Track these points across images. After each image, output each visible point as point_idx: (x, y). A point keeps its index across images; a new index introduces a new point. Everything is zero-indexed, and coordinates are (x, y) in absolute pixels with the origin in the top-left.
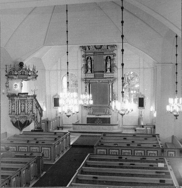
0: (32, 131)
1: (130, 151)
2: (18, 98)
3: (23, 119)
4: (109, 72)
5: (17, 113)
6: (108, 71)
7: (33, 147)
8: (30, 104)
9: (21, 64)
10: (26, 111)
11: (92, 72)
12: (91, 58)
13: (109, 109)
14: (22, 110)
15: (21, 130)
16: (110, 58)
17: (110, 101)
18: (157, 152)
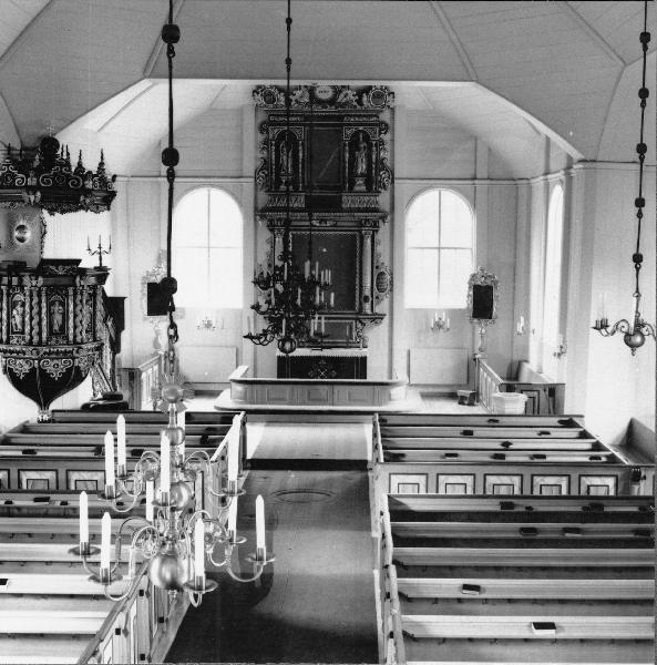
0: (86, 408)
1: (516, 480)
2: (40, 279)
3: (56, 361)
4: (364, 188)
5: (36, 339)
6: (360, 185)
7: (590, 478)
8: (87, 301)
10: (71, 331)
13: (359, 325)
14: (56, 328)
15: (43, 403)
16: (367, 138)
17: (366, 299)
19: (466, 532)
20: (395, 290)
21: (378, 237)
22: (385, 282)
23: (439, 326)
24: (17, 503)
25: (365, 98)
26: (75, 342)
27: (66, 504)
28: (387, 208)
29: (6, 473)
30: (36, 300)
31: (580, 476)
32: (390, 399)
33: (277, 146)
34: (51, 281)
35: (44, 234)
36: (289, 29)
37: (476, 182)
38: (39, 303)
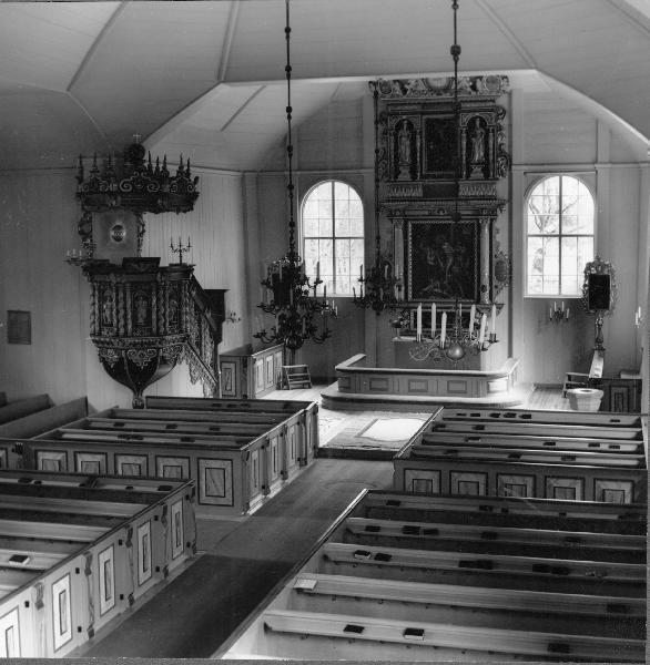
1: (481, 479)
4: (408, 177)
5: (122, 331)
6: (477, 172)
9: (136, 152)
11: (414, 178)
12: (482, 120)
18: (487, 478)
19: (470, 534)
21: (497, 225)
24: (137, 489)
26: (158, 334)
27: (507, 511)
29: (64, 454)
30: (121, 295)
31: (199, 458)
33: (396, 136)
34: (134, 278)
35: (141, 234)
36: (288, 37)
37: (596, 166)
38: (125, 298)
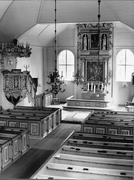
1: (104, 129)
5: (11, 89)
6: (104, 48)
16: (106, 35)
20: (113, 76)
21: (109, 62)
22: (111, 75)
23: (125, 86)
24: (14, 130)
25: (105, 25)
28: (112, 55)
30: (11, 79)
32: (106, 106)
38: (12, 80)
